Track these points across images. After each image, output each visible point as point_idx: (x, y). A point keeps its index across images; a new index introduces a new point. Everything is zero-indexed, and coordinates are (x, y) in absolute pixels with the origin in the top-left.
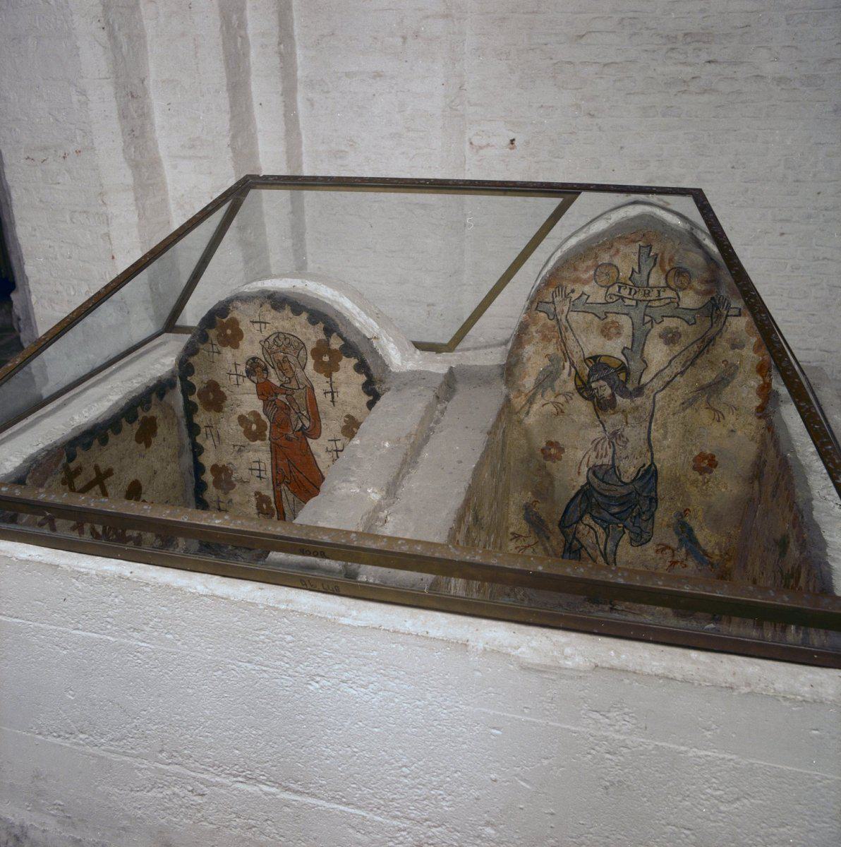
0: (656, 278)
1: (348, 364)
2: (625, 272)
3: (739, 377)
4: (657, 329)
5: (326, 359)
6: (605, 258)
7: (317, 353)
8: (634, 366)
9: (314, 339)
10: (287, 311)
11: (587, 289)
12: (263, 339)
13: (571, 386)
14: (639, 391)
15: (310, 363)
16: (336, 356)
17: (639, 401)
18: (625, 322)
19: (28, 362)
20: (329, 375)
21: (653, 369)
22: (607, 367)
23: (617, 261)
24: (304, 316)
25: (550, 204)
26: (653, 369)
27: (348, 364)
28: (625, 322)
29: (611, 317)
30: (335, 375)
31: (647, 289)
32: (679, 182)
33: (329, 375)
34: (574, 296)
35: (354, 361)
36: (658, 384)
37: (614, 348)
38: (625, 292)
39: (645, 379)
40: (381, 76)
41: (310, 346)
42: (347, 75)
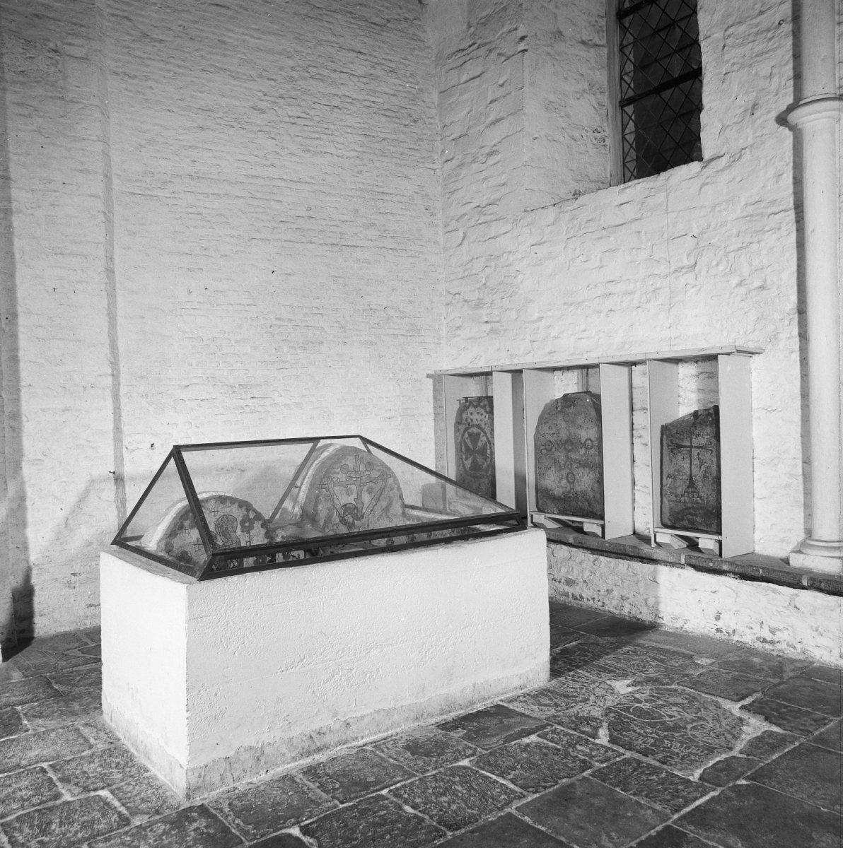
0: (362, 468)
1: (257, 525)
2: (351, 466)
3: (394, 502)
4: (365, 488)
5: (247, 524)
6: (343, 462)
7: (242, 523)
8: (359, 506)
9: (241, 515)
10: (228, 503)
11: (339, 476)
12: (216, 520)
13: (338, 520)
14: (362, 516)
15: (239, 530)
16: (252, 522)
17: (363, 520)
18: (354, 487)
19: (446, 497)
20: (248, 533)
21: (366, 506)
22: (350, 508)
23: (348, 463)
24: (237, 504)
25: (309, 446)
26: (366, 506)
27: (257, 525)
28: (354, 487)
29: (349, 486)
30: (251, 532)
31: (359, 472)
32: (308, 433)
33: (248, 533)
34: (335, 480)
35: (261, 522)
36: (368, 512)
37: (351, 500)
38: (352, 475)
39: (364, 511)
40: (68, 410)
41: (240, 519)
42: (43, 410)
